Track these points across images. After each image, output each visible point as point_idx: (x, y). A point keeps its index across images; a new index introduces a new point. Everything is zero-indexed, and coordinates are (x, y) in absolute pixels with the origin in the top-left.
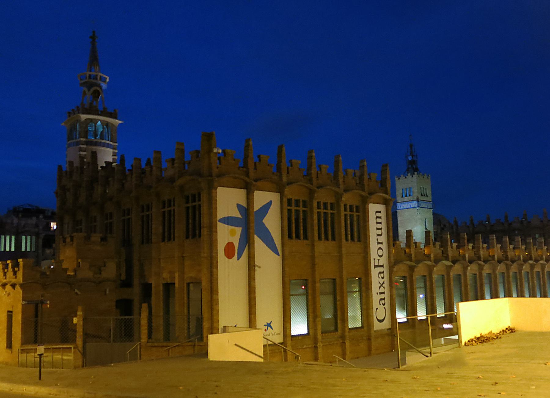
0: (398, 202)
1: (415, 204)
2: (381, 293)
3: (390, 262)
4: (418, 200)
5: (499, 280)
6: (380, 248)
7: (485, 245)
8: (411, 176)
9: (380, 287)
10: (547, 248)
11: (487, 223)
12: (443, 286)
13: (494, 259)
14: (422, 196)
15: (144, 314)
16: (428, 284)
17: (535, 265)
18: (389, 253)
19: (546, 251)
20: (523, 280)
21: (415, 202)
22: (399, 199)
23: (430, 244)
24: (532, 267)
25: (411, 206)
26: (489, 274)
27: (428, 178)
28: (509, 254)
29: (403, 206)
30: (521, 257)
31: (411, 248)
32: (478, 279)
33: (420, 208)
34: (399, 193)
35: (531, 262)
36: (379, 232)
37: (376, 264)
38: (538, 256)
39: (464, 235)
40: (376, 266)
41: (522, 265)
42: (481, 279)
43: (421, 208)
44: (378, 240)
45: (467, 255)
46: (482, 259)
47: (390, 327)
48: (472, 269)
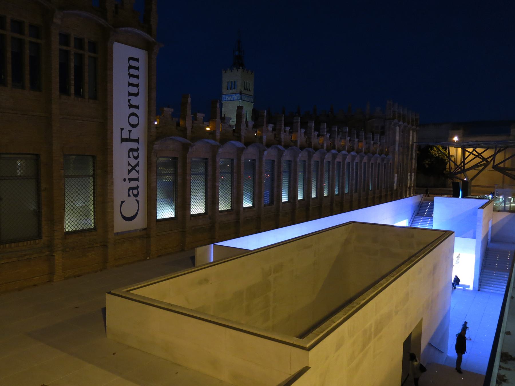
0: (223, 94)
1: (238, 96)
2: (131, 180)
3: (149, 136)
4: (241, 93)
5: (300, 168)
6: (133, 114)
7: (288, 129)
8: (236, 70)
9: (130, 171)
10: (349, 139)
11: (297, 114)
12: (232, 173)
13: (296, 145)
14: (245, 90)
15: (413, 167)
16: (210, 169)
17: (337, 154)
18: (150, 123)
19: (349, 141)
20: (324, 170)
21: (238, 95)
22: (224, 91)
23: (216, 118)
24: (334, 156)
25: (234, 98)
26: (289, 161)
27: (252, 74)
28: (312, 141)
29: (228, 97)
30: (325, 145)
31: (187, 119)
32: (276, 167)
33: (242, 101)
34: (225, 85)
35: (333, 151)
36: (134, 90)
37: (123, 137)
38: (341, 146)
39: (264, 113)
40: (123, 140)
41: (324, 154)
42: (279, 167)
43: (243, 101)
44: (131, 102)
45: (265, 137)
46: (283, 144)
47: (146, 227)
48: (270, 154)
